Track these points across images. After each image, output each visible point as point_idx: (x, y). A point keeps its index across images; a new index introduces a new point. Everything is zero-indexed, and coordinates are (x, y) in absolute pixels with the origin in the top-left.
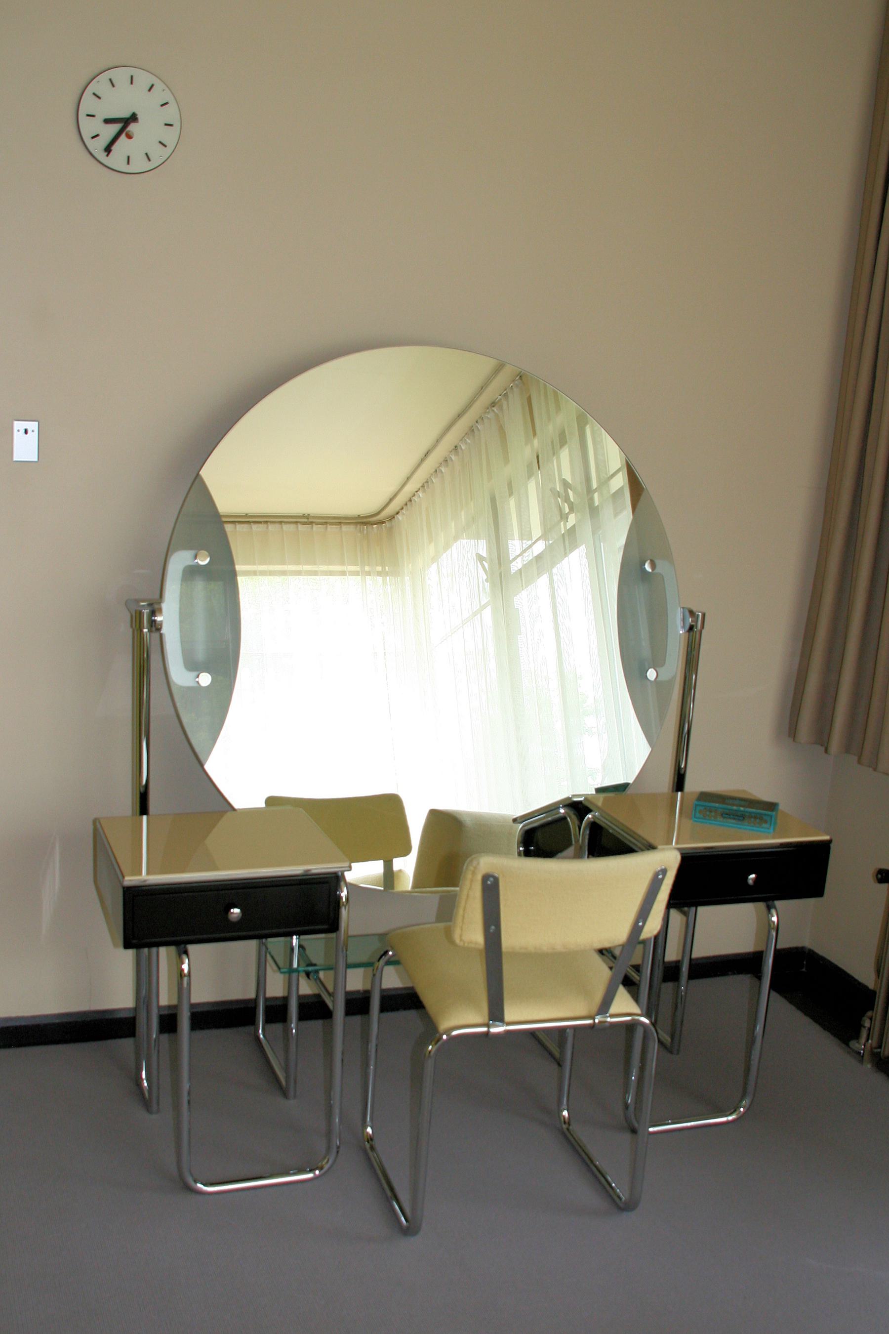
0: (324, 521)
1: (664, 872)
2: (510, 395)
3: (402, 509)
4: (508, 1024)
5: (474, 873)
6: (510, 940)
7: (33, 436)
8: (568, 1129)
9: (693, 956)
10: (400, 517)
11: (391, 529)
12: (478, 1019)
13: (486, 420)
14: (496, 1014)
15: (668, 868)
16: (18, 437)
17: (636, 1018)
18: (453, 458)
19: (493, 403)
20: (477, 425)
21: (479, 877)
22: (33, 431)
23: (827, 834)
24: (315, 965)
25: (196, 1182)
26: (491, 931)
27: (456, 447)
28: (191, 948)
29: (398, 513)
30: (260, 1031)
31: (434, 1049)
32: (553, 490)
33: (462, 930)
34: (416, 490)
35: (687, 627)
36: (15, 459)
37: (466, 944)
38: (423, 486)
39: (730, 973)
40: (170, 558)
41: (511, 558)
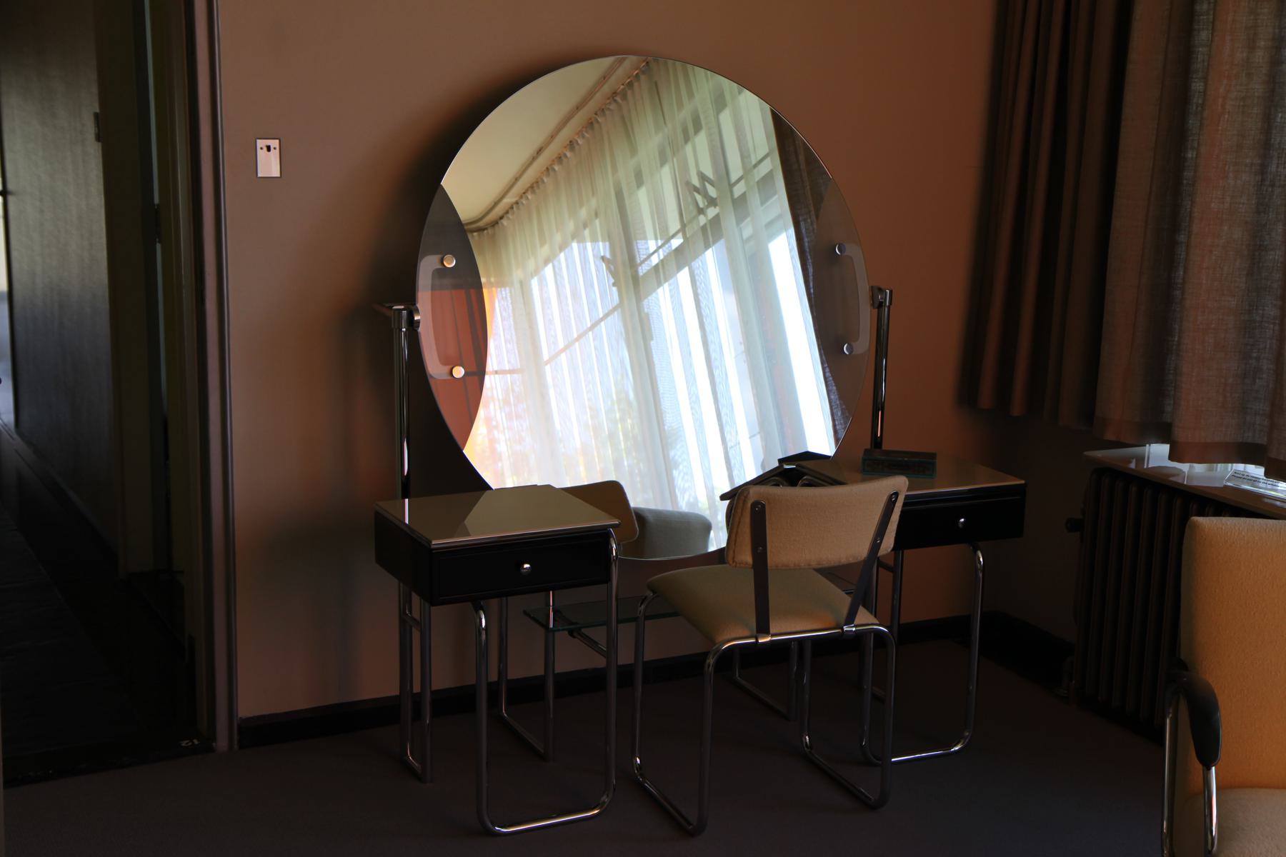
1: (896, 494)
2: (636, 84)
4: (773, 635)
5: (745, 501)
6: (779, 554)
7: (275, 155)
8: (810, 752)
9: (901, 622)
10: (505, 222)
11: (493, 236)
12: (747, 633)
13: (607, 112)
14: (763, 628)
16: (262, 154)
18: (568, 154)
19: (614, 93)
20: (597, 117)
22: (275, 148)
24: (576, 623)
26: (759, 551)
27: (571, 142)
29: (501, 218)
30: (504, 711)
32: (688, 183)
33: (734, 552)
34: (524, 191)
35: (877, 305)
36: (259, 175)
40: (421, 261)
41: (638, 261)
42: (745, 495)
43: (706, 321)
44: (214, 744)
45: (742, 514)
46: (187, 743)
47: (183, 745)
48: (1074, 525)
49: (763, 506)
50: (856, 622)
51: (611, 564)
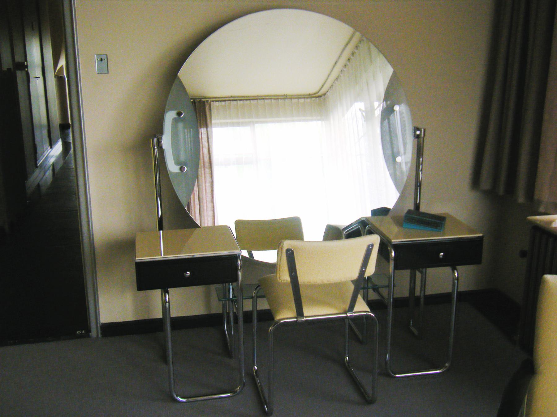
0: (277, 97)
1: (372, 245)
3: (329, 90)
6: (302, 278)
10: (328, 93)
12: (292, 315)
15: (374, 244)
17: (368, 313)
21: (284, 251)
23: (481, 233)
25: (177, 397)
28: (170, 290)
29: (327, 92)
31: (272, 329)
37: (282, 281)
38: (337, 78)
39: (26, 182)
42: (281, 245)
43: (209, 140)
44: (90, 334)
45: (281, 255)
46: (79, 332)
47: (77, 333)
48: (523, 254)
49: (293, 251)
50: (355, 310)
51: (238, 271)
